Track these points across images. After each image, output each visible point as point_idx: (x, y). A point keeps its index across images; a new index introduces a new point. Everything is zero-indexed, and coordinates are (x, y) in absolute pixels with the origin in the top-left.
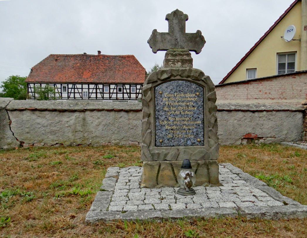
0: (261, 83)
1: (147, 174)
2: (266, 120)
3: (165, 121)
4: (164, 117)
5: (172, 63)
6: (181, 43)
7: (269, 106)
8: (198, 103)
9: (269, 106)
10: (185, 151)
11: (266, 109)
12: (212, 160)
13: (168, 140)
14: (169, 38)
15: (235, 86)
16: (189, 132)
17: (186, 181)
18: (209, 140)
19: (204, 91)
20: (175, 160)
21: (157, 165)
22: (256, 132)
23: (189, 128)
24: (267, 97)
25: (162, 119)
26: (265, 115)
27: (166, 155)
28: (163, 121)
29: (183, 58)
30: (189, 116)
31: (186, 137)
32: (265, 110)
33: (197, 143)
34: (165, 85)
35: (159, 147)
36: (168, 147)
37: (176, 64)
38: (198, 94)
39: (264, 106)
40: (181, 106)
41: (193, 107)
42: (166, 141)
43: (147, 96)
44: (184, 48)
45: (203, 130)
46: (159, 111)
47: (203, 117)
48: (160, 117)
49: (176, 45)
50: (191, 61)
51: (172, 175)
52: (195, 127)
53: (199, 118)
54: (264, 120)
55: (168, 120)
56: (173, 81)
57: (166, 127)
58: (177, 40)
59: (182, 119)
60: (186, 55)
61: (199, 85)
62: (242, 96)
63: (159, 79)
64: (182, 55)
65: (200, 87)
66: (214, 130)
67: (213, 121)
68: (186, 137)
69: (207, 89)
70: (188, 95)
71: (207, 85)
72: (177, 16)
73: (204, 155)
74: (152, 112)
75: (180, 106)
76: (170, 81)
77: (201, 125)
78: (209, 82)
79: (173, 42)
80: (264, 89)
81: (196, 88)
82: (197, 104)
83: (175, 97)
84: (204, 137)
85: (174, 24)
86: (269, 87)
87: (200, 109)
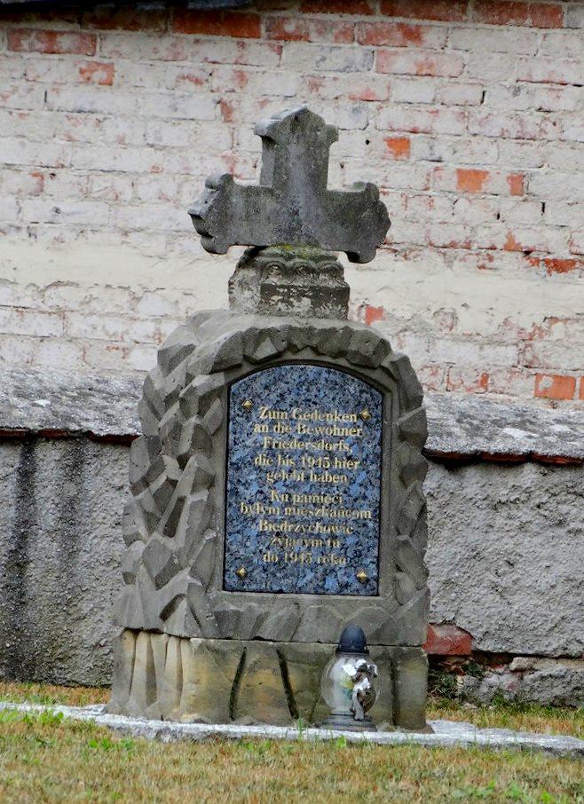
0: (413, 35)
1: (204, 681)
2: (534, 528)
3: (258, 504)
4: (254, 488)
5: (282, 301)
6: (310, 227)
7: (558, 428)
8: (366, 444)
9: (558, 421)
10: (319, 610)
11: (540, 451)
12: (406, 645)
13: (265, 570)
14: (269, 204)
15: (65, 42)
16: (332, 544)
17: (359, 687)
18: (399, 575)
19: (388, 404)
20: (289, 638)
21: (234, 651)
22: (467, 609)
23: (331, 531)
24: (483, 238)
25: (248, 498)
26: (528, 492)
27: (260, 620)
28: (251, 503)
29: (317, 283)
30: (335, 489)
31: (321, 564)
32: (530, 457)
33: (356, 585)
34: (263, 378)
35: (235, 593)
36: (265, 595)
37: (296, 303)
38: (365, 413)
39: (521, 426)
40: (311, 455)
41: (349, 458)
42: (258, 574)
43: (208, 414)
44: (316, 245)
45: (376, 541)
46: (238, 469)
47: (377, 495)
48: (241, 489)
49: (291, 232)
50: (343, 294)
51: (281, 687)
52: (350, 530)
53: (365, 497)
54: (522, 527)
55: (266, 500)
56: (288, 367)
57: (261, 525)
58: (297, 213)
59: (310, 497)
60: (326, 271)
61: (371, 382)
62: (147, 189)
63: (246, 358)
64: (313, 271)
65: (373, 390)
66: (414, 543)
67: (412, 510)
68: (321, 564)
69: (396, 397)
70: (334, 417)
71: (399, 387)
72: (303, 129)
73: (378, 626)
74: (219, 470)
75: (306, 454)
76: (279, 365)
77: (371, 525)
78: (406, 378)
79: (284, 220)
80: (447, 123)
81: (361, 392)
82: (362, 449)
83: (292, 421)
84: (378, 566)
85: (293, 159)
86: (523, 101)
87: (371, 468)
